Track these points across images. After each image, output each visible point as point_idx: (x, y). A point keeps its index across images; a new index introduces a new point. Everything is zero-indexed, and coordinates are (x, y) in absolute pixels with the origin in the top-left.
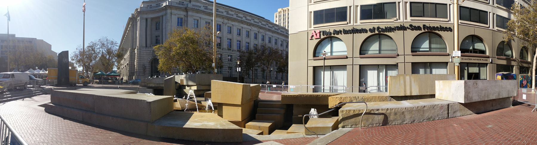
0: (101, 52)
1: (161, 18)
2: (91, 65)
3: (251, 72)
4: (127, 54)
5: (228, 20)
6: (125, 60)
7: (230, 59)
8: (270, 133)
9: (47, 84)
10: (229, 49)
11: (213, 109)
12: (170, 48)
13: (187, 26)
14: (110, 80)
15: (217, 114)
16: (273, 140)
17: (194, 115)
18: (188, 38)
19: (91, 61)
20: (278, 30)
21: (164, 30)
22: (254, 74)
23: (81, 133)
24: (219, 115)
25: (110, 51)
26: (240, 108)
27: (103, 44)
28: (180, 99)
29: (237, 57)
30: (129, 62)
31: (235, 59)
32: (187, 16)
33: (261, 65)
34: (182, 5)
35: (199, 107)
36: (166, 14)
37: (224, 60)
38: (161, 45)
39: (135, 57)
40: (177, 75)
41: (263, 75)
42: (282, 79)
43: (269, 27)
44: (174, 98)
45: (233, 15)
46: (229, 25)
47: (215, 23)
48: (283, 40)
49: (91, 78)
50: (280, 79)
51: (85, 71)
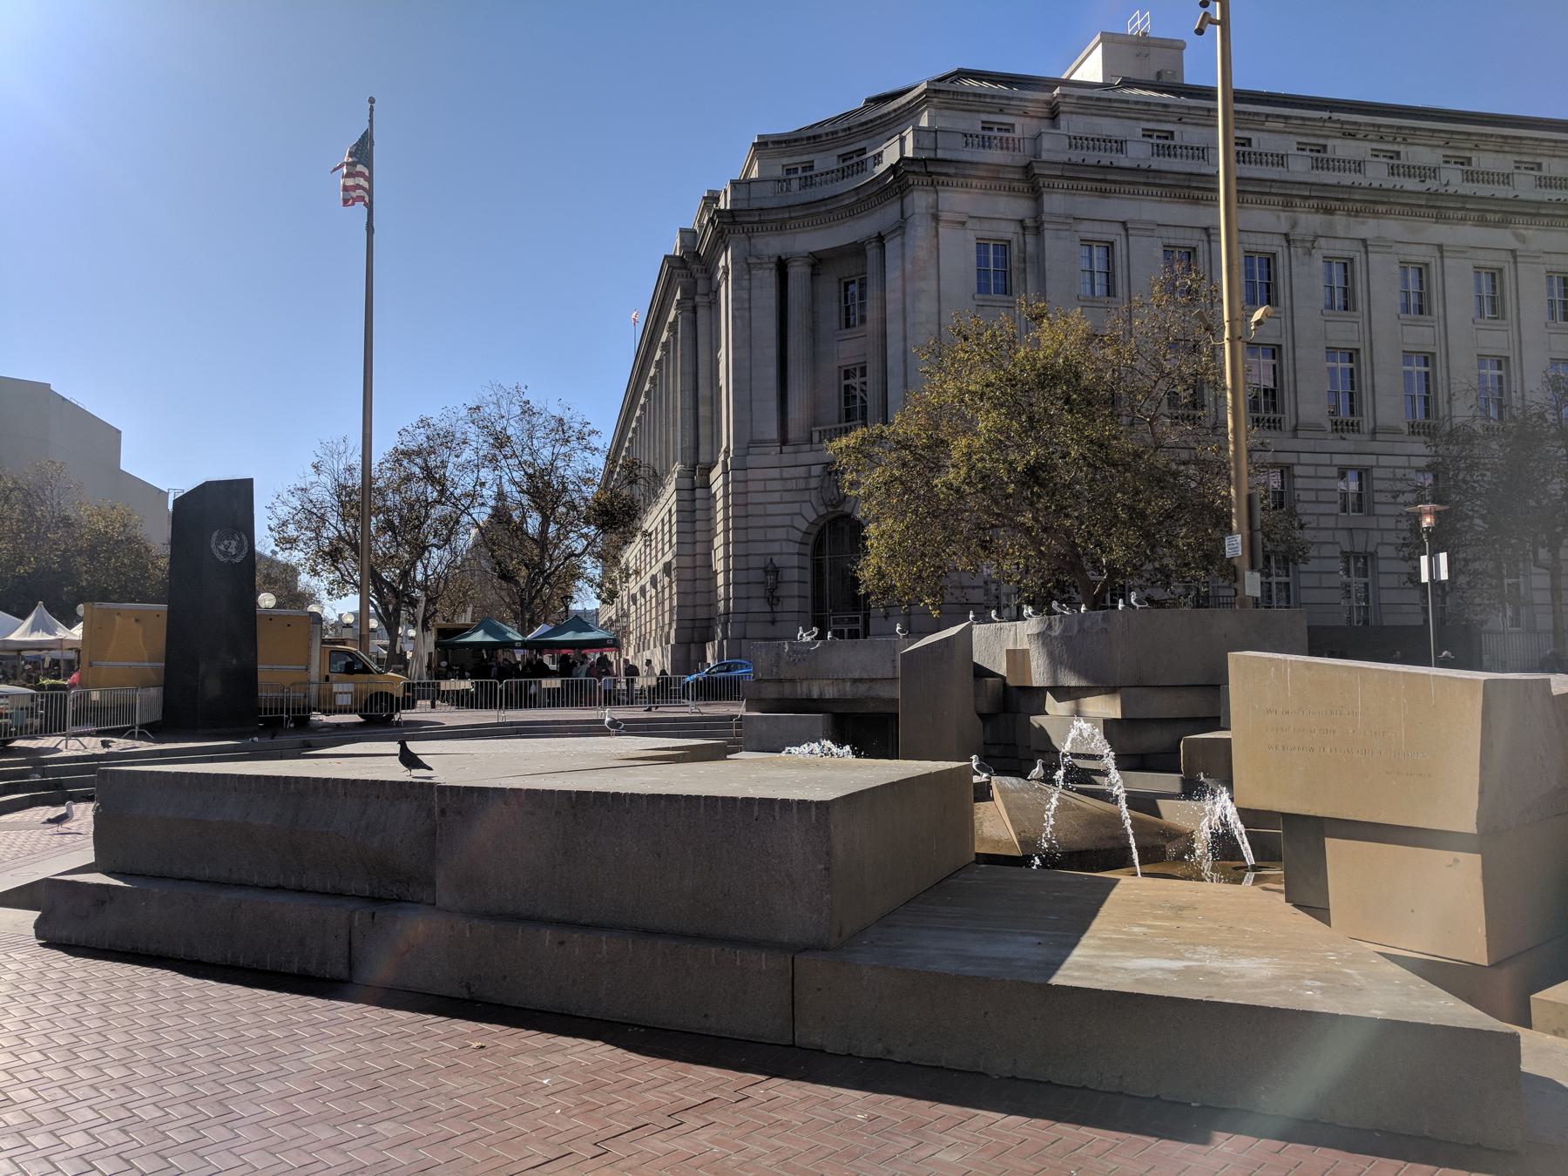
0: (486, 492)
1: (872, 252)
2: (419, 577)
4: (662, 501)
5: (1329, 211)
7: (1351, 499)
9: (75, 723)
11: (1250, 859)
13: (1042, 292)
14: (550, 674)
17: (1114, 894)
18: (1047, 378)
19: (420, 550)
23: (335, 1074)
25: (548, 484)
28: (1010, 782)
29: (1411, 474)
30: (677, 555)
31: (1396, 494)
32: (1035, 227)
36: (901, 226)
37: (1310, 508)
38: (876, 429)
39: (710, 520)
45: (1359, 166)
46: (1339, 244)
47: (1235, 243)
49: (418, 671)
51: (374, 624)
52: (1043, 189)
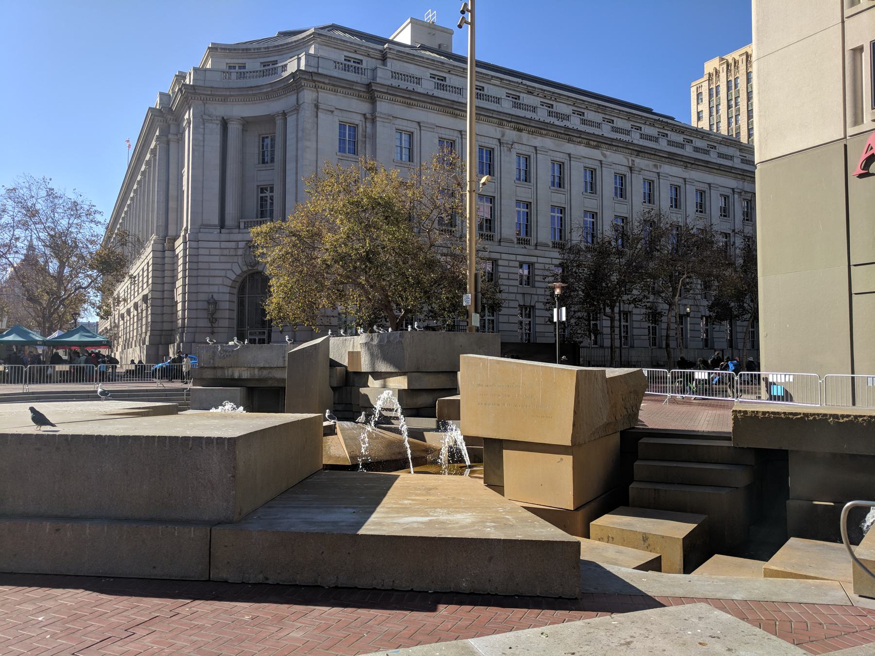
1: (279, 122)
3: (607, 323)
4: (143, 257)
6: (133, 283)
7: (525, 278)
8: (689, 567)
10: (523, 242)
11: (468, 463)
12: (317, 235)
15: (482, 481)
16: (706, 600)
17: (397, 483)
18: (376, 204)
20: (706, 152)
21: (290, 166)
22: (617, 331)
24: (489, 486)
25: (65, 242)
26: (568, 460)
27: (32, 213)
28: (347, 424)
29: (552, 267)
30: (152, 291)
32: (372, 118)
33: (645, 296)
34: (357, 70)
35: (418, 454)
36: (297, 108)
37: (505, 282)
38: (278, 223)
39: (174, 270)
40: (336, 334)
41: (654, 333)
42: (731, 346)
43: (671, 143)
44: (326, 420)
45: (534, 109)
48: (728, 192)
50: (725, 345)
52: (377, 99)
